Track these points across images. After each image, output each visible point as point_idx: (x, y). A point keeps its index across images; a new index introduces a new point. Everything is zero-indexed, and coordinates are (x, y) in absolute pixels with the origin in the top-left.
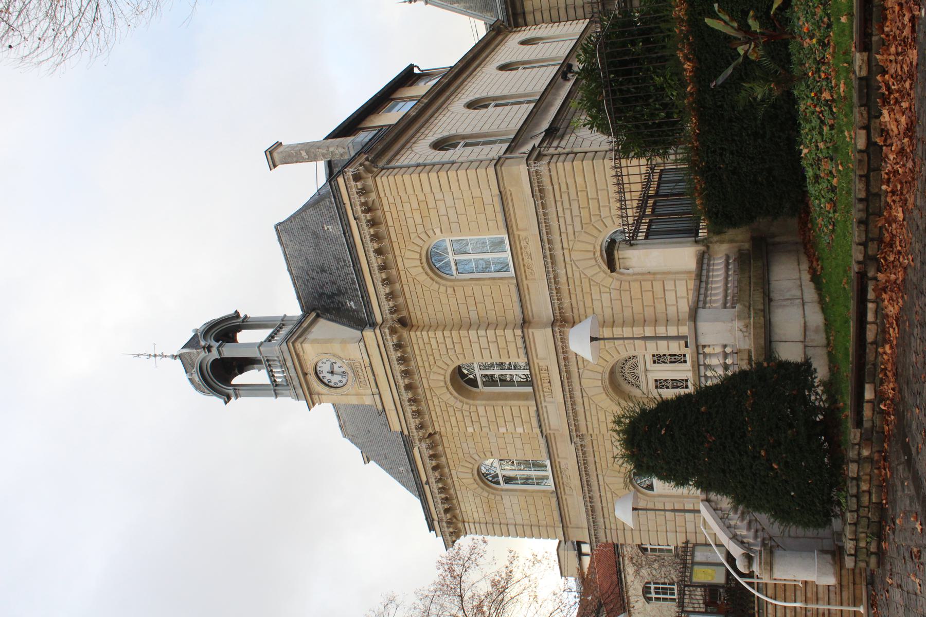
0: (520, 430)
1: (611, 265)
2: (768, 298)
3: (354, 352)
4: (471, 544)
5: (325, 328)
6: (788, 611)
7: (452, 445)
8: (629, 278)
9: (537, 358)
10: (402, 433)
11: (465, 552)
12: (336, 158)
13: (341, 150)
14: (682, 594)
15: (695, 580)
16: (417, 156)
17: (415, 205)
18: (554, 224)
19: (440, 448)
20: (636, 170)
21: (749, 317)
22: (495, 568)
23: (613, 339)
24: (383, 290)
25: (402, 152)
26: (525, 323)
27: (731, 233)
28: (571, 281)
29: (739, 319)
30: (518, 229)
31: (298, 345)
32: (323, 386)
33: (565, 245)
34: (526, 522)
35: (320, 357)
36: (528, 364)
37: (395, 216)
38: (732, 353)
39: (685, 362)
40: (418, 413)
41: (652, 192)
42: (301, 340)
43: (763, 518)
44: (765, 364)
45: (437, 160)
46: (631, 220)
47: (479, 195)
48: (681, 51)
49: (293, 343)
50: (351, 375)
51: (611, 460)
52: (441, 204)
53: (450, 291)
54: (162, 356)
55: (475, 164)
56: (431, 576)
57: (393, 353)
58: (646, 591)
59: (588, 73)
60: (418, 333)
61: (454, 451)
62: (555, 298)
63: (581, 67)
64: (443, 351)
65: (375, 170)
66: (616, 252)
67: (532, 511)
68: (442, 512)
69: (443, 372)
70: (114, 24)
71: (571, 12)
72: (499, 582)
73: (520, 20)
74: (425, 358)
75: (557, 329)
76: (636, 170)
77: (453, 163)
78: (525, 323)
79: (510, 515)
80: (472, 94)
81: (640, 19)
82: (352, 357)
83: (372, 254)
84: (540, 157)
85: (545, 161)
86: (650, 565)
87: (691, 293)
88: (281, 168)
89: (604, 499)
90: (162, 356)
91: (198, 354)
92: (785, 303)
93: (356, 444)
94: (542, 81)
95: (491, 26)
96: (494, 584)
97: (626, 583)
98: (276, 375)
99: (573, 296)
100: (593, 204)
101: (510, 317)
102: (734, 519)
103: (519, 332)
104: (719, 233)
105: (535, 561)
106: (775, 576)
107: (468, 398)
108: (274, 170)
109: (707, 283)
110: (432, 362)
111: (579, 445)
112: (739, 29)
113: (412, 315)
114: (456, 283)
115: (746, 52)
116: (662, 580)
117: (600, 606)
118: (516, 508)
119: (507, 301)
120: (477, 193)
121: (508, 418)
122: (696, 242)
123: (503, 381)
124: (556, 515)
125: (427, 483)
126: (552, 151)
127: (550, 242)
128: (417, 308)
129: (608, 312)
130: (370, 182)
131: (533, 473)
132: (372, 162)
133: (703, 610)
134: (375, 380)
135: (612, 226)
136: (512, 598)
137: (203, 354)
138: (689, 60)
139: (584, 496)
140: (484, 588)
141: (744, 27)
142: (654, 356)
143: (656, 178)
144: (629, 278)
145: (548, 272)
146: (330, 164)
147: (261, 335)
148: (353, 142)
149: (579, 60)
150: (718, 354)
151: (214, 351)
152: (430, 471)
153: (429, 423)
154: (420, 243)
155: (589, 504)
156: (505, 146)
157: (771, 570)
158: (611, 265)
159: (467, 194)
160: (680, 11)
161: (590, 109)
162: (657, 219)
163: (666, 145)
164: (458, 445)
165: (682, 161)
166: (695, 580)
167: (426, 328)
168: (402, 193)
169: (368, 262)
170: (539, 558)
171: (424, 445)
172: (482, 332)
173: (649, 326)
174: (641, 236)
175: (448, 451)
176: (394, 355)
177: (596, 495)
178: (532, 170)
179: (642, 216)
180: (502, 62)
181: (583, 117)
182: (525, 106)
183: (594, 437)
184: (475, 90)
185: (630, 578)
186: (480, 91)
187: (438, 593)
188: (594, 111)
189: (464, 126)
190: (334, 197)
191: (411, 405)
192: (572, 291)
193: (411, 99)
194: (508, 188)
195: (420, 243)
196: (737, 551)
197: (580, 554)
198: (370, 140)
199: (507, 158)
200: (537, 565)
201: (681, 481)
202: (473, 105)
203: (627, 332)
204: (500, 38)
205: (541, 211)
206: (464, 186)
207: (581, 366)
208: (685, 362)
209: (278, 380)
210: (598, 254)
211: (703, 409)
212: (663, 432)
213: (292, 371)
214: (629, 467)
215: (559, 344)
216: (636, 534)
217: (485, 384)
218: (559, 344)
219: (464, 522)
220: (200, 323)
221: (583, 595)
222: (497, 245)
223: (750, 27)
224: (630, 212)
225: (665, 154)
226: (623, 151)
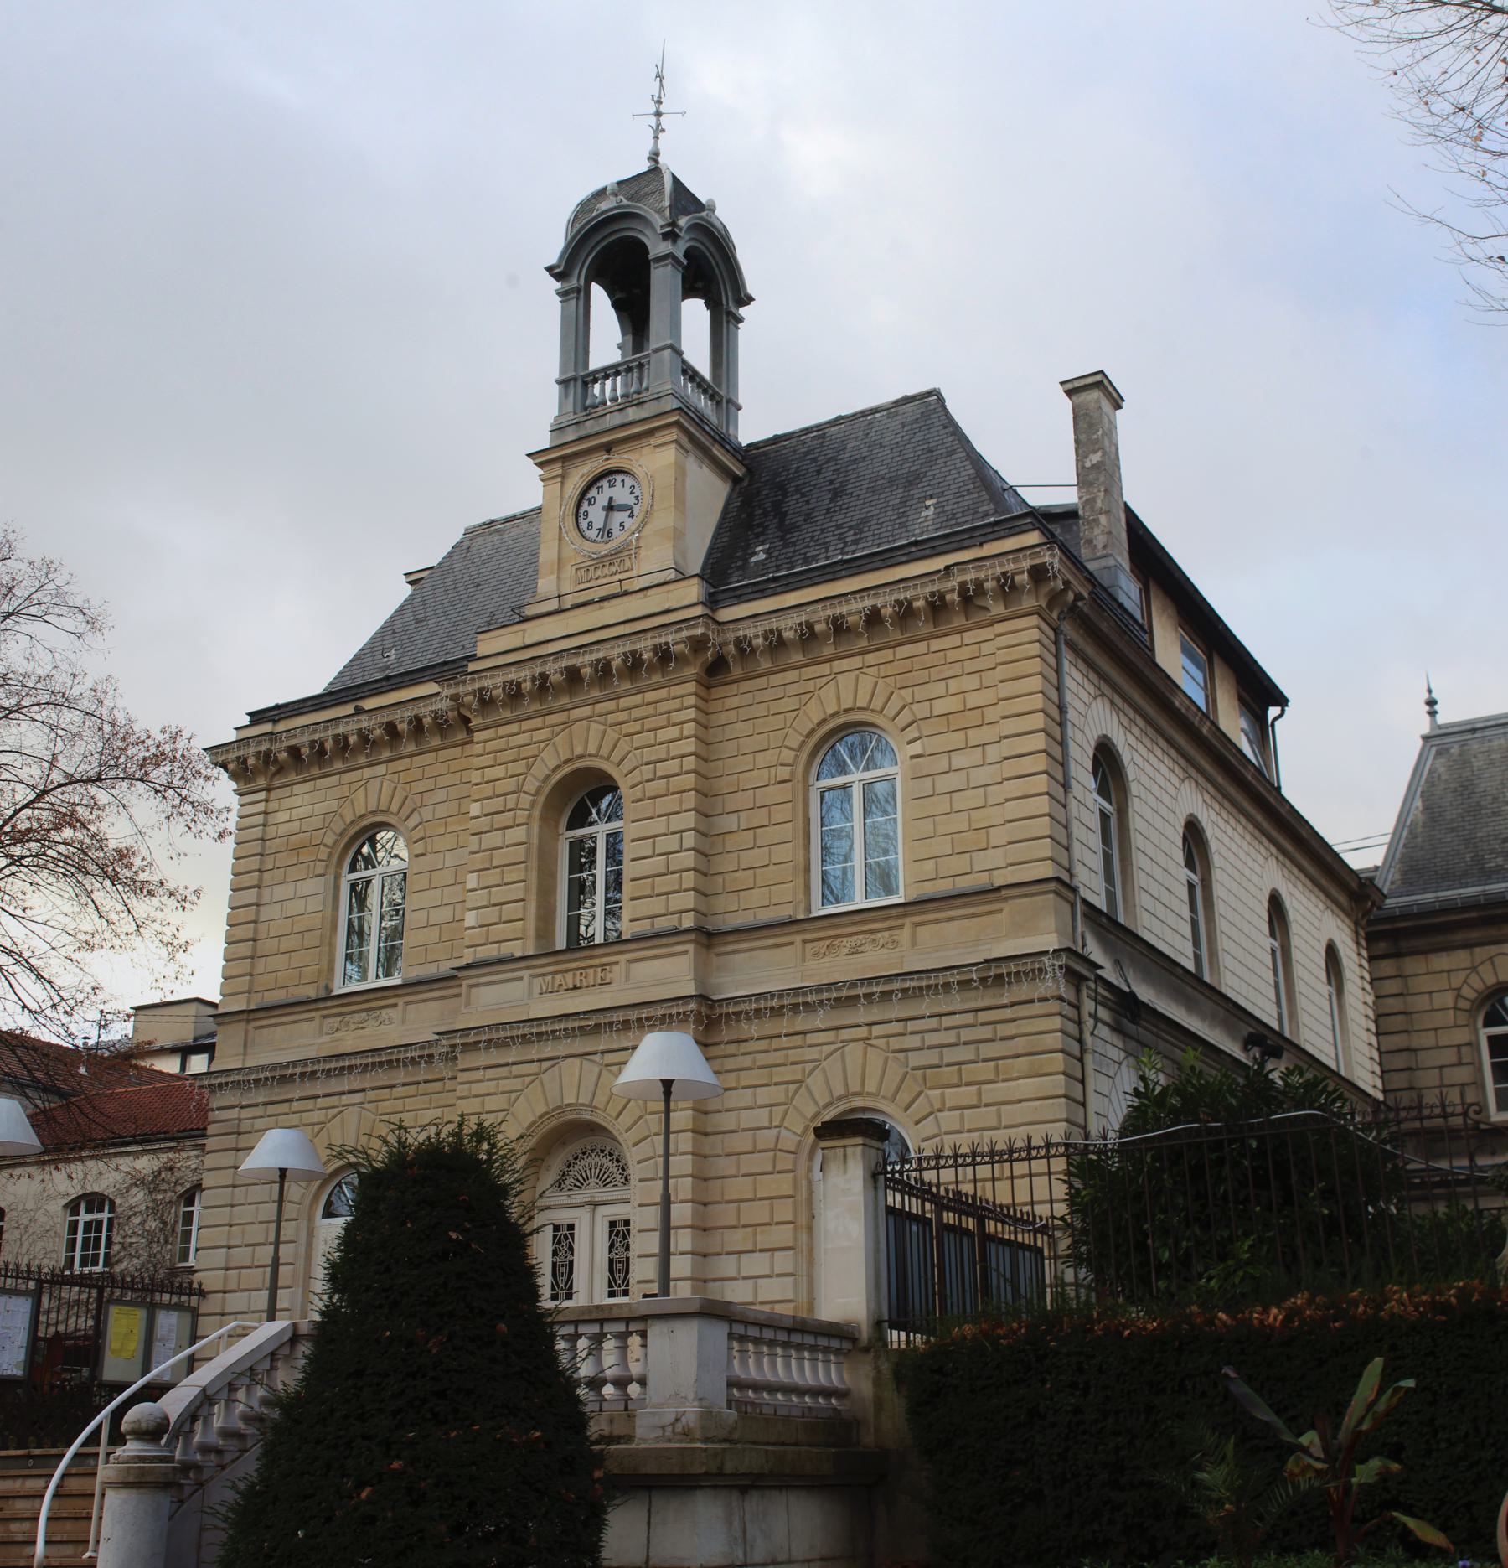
0: (471, 919)
1: (834, 1130)
2: (746, 1484)
3: (655, 558)
4: (218, 805)
5: (709, 494)
6: (26, 1526)
7: (443, 768)
8: (802, 1171)
10: (473, 658)
11: (200, 791)
12: (1084, 531)
13: (1100, 540)
14: (83, 1281)
15: (114, 1311)
16: (1082, 708)
17: (974, 700)
18: (925, 1006)
19: (436, 741)
20: (1041, 1193)
21: (706, 1440)
22: (160, 857)
23: (667, 1132)
24: (788, 626)
25: (1092, 676)
26: (708, 937)
27: (896, 1403)
28: (798, 1040)
29: (702, 1414)
30: (916, 925)
31: (673, 434)
34: (262, 927)
35: (645, 483)
36: (619, 941)
38: (627, 1399)
39: (612, 1294)
40: (515, 694)
41: (992, 1227)
42: (685, 440)
43: (249, 1466)
44: (598, 1474)
45: (1074, 751)
46: (930, 1176)
47: (993, 843)
48: (1310, 1302)
49: (677, 424)
50: (605, 549)
51: (395, 1118)
52: (975, 756)
53: (784, 773)
54: (658, 130)
55: (1061, 836)
56: (147, 712)
57: (650, 643)
58: (95, 1201)
59: (1260, 1091)
60: (692, 700)
61: (428, 773)
62: (762, 1004)
63: (1275, 1076)
64: (650, 754)
65: (1055, 615)
66: (859, 1140)
67: (286, 944)
68: (293, 742)
69: (604, 751)
70: (1400, 40)
71: (1400, 1061)
72: (129, 866)
73: (1382, 947)
74: (636, 713)
75: (692, 1006)
76: (1041, 1193)
77: (1066, 786)
78: (708, 937)
79: (281, 892)
80: (1219, 833)
81: (1381, 1213)
82: (642, 553)
83: (868, 603)
84: (1075, 979)
85: (1063, 989)
86: (154, 1210)
87: (767, 1308)
88: (1066, 405)
89: (309, 1104)
90: (658, 130)
91: (660, 211)
92: (736, 1523)
93: (450, 555)
94: (1244, 989)
95: (1371, 880)
96: (123, 855)
97: (116, 1155)
98: (608, 383)
99: (763, 1045)
100: (967, 1094)
101: (721, 903)
102: (247, 1400)
103: (688, 922)
104: (899, 1376)
105: (175, 947)
106: (110, 1493)
107: (546, 805)
108: (1060, 389)
109: (786, 1345)
110: (627, 728)
111: (433, 1050)
112: (1357, 1435)
114: (800, 786)
115: (1305, 1450)
116: (117, 1239)
117: (62, 1095)
118: (296, 907)
119: (756, 897)
120: (998, 836)
121: (499, 894)
122: (878, 1325)
123: (580, 891)
124: (278, 996)
125: (360, 711)
126: (1088, 1005)
128: (748, 699)
129: (728, 1121)
130: (1028, 602)
131: (373, 946)
132: (1073, 608)
133: (41, 1334)
134: (592, 602)
135: (915, 1136)
136: (89, 894)
137: (659, 221)
138: (1288, 1319)
139: (317, 1060)
140: (116, 831)
141: (1360, 1448)
142: (627, 1223)
143: (1024, 1238)
144: (802, 1171)
145: (819, 989)
146: (1068, 516)
147: (697, 348)
148: (1118, 566)
149: (1289, 1073)
150: (627, 1368)
151: (664, 247)
152: (385, 718)
153: (492, 718)
154: (891, 710)
155: (298, 1070)
156: (1100, 902)
157: (126, 1485)
158: (834, 1130)
159: (995, 815)
160: (1400, 1302)
161: (1178, 1091)
162: (931, 1238)
163: (1094, 1261)
164: (441, 782)
165: (1060, 1296)
166: (114, 1311)
167: (702, 718)
168: (1002, 671)
169: (852, 594)
170: (180, 955)
171: (443, 705)
172: (690, 839)
173: (695, 1213)
174: (895, 1199)
175: (429, 758)
176: (645, 646)
177: (318, 1088)
178: (1046, 961)
179: (941, 1204)
180: (1289, 903)
181: (1162, 1079)
182: (1189, 949)
183: (449, 1085)
184: (1226, 840)
185: (126, 1163)
186: (1224, 851)
187: (107, 728)
188: (1175, 1101)
189: (1147, 813)
190: (996, 523)
191: (533, 679)
192: (776, 1043)
193: (1211, 698)
194: (1007, 907)
195: (891, 710)
196: (174, 1404)
197: (185, 1051)
198: (1121, 606)
199: (1073, 905)
200: (164, 952)
201: (339, 1275)
202: (1193, 834)
203: (682, 1164)
204: (1343, 899)
205: (954, 977)
206: (1014, 809)
207: (609, 1058)
208: (612, 1294)
209: (597, 387)
210: (857, 1103)
211: (502, 1326)
212: (454, 1235)
213: (617, 419)
214: (379, 1157)
215: (660, 1011)
216: (225, 1178)
217: (577, 846)
218: (660, 1011)
219: (268, 790)
220: (728, 216)
221: (91, 1056)
222: (883, 878)
223: (1363, 1461)
224: (947, 1175)
225: (1077, 1260)
226: (1084, 1164)
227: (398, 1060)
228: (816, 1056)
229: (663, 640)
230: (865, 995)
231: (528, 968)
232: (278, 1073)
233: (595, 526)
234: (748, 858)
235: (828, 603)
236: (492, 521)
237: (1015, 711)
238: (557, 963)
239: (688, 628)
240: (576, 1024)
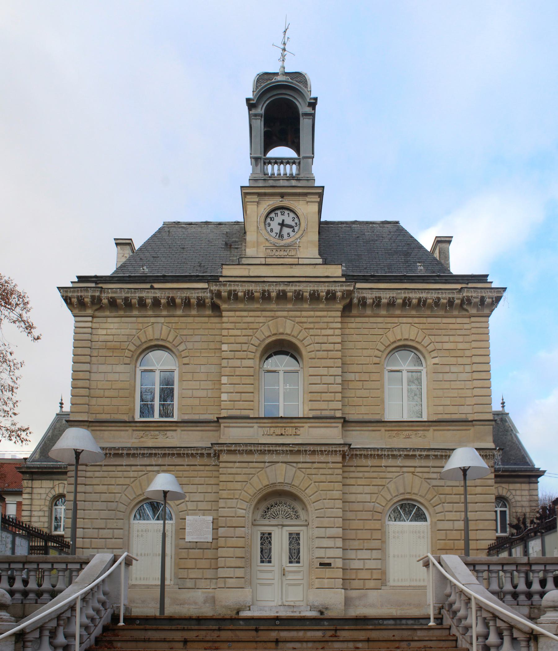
9: (309, 427)
10: (222, 276)
26: (345, 422)
32: (268, 210)
33: (418, 470)
89: (128, 468)
113: (352, 320)
119: (363, 410)
125: (152, 288)
127: (427, 457)
128: (359, 325)
155: (125, 452)
168: (474, 337)
175: (190, 320)
227: (184, 454)
228: (391, 477)
231: (257, 423)
233: (275, 231)
234: (359, 393)
236: (179, 222)
237: (479, 354)
238: (272, 423)
239: (346, 286)
240: (288, 449)
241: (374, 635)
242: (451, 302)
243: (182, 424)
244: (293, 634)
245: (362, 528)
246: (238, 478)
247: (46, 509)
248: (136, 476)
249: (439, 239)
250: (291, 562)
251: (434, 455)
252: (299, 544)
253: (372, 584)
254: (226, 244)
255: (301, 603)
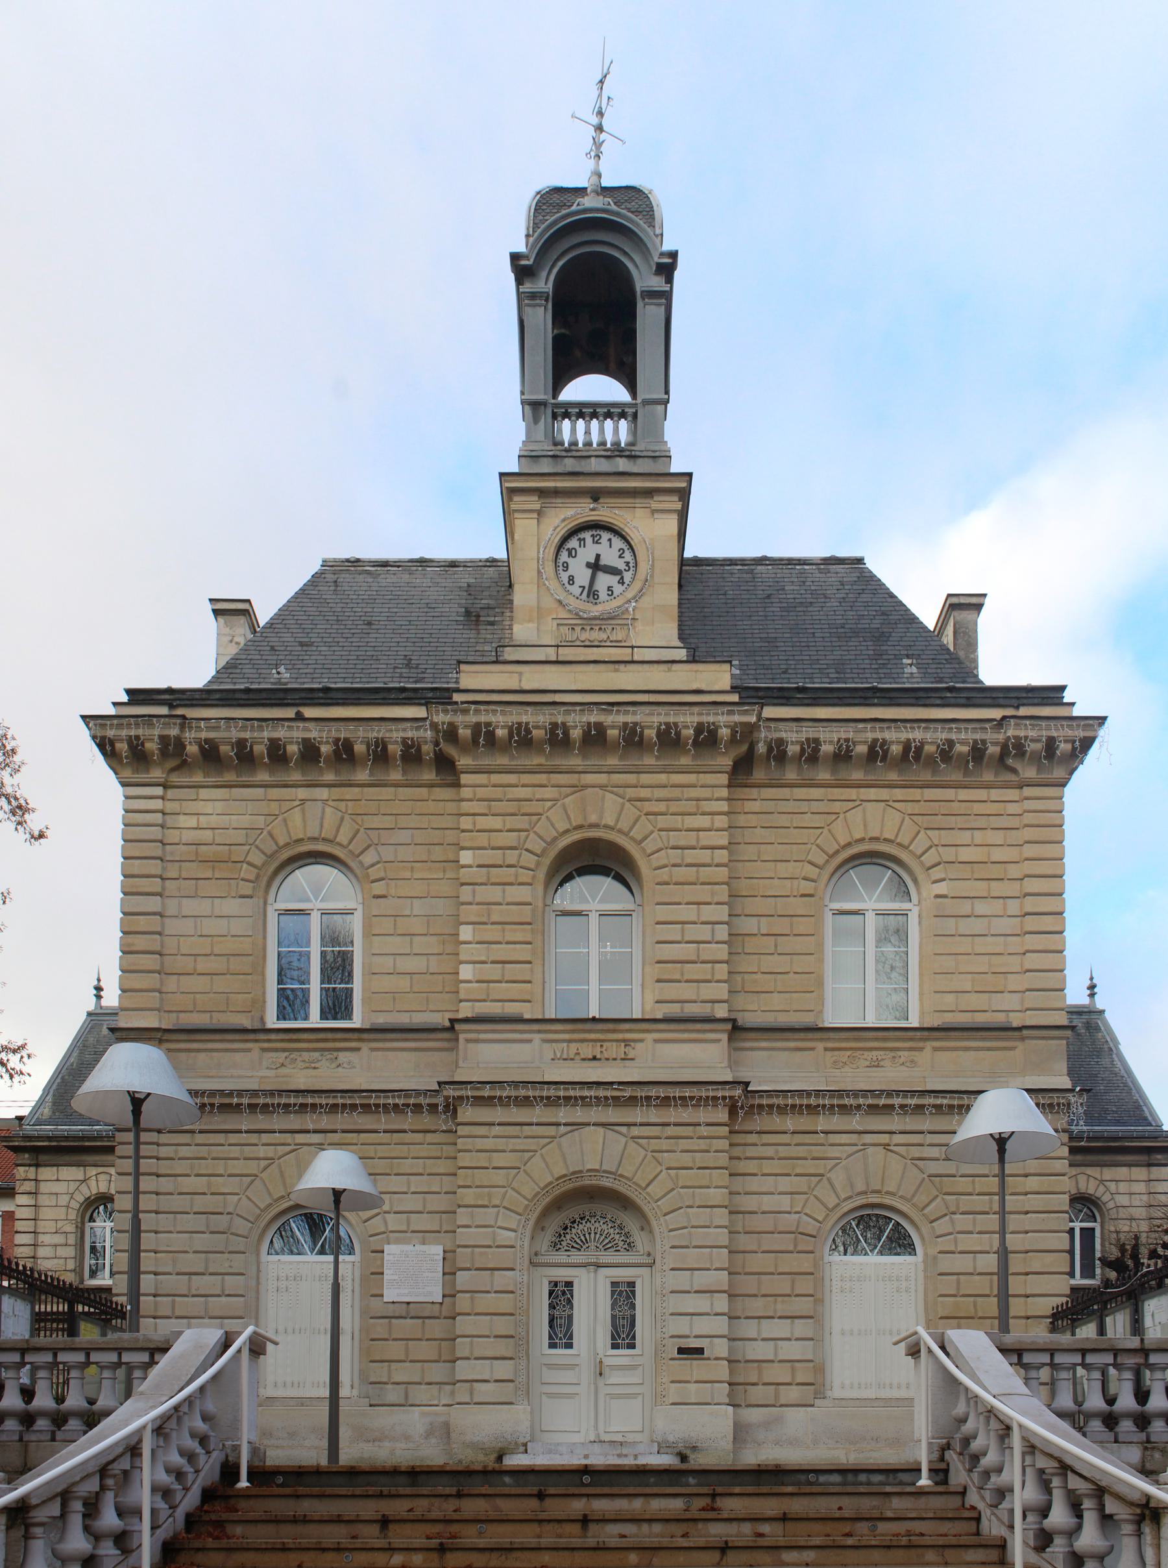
10: (458, 690)
17: (998, 854)
26: (736, 1029)
33: (898, 1138)
37: (978, 808)
52: (996, 907)
64: (675, 838)
79: (190, 906)
113: (754, 793)
125: (300, 717)
127: (920, 1108)
159: (1014, 963)
168: (1029, 834)
176: (577, 723)
215: (653, 1092)
218: (662, 1092)
229: (711, 719)
230: (768, 1106)
231: (539, 1032)
232: (217, 1101)
235: (878, 725)
236: (358, 560)
238: (573, 1031)
240: (609, 1094)
241: (797, 1506)
242: (978, 752)
243: (372, 1036)
244: (621, 1505)
245: (772, 1270)
246: (499, 1160)
247: (70, 1228)
248: (270, 1155)
249: (955, 600)
250: (615, 1346)
251: (934, 1106)
252: (633, 1306)
253: (792, 1394)
254: (468, 613)
255: (638, 1437)
